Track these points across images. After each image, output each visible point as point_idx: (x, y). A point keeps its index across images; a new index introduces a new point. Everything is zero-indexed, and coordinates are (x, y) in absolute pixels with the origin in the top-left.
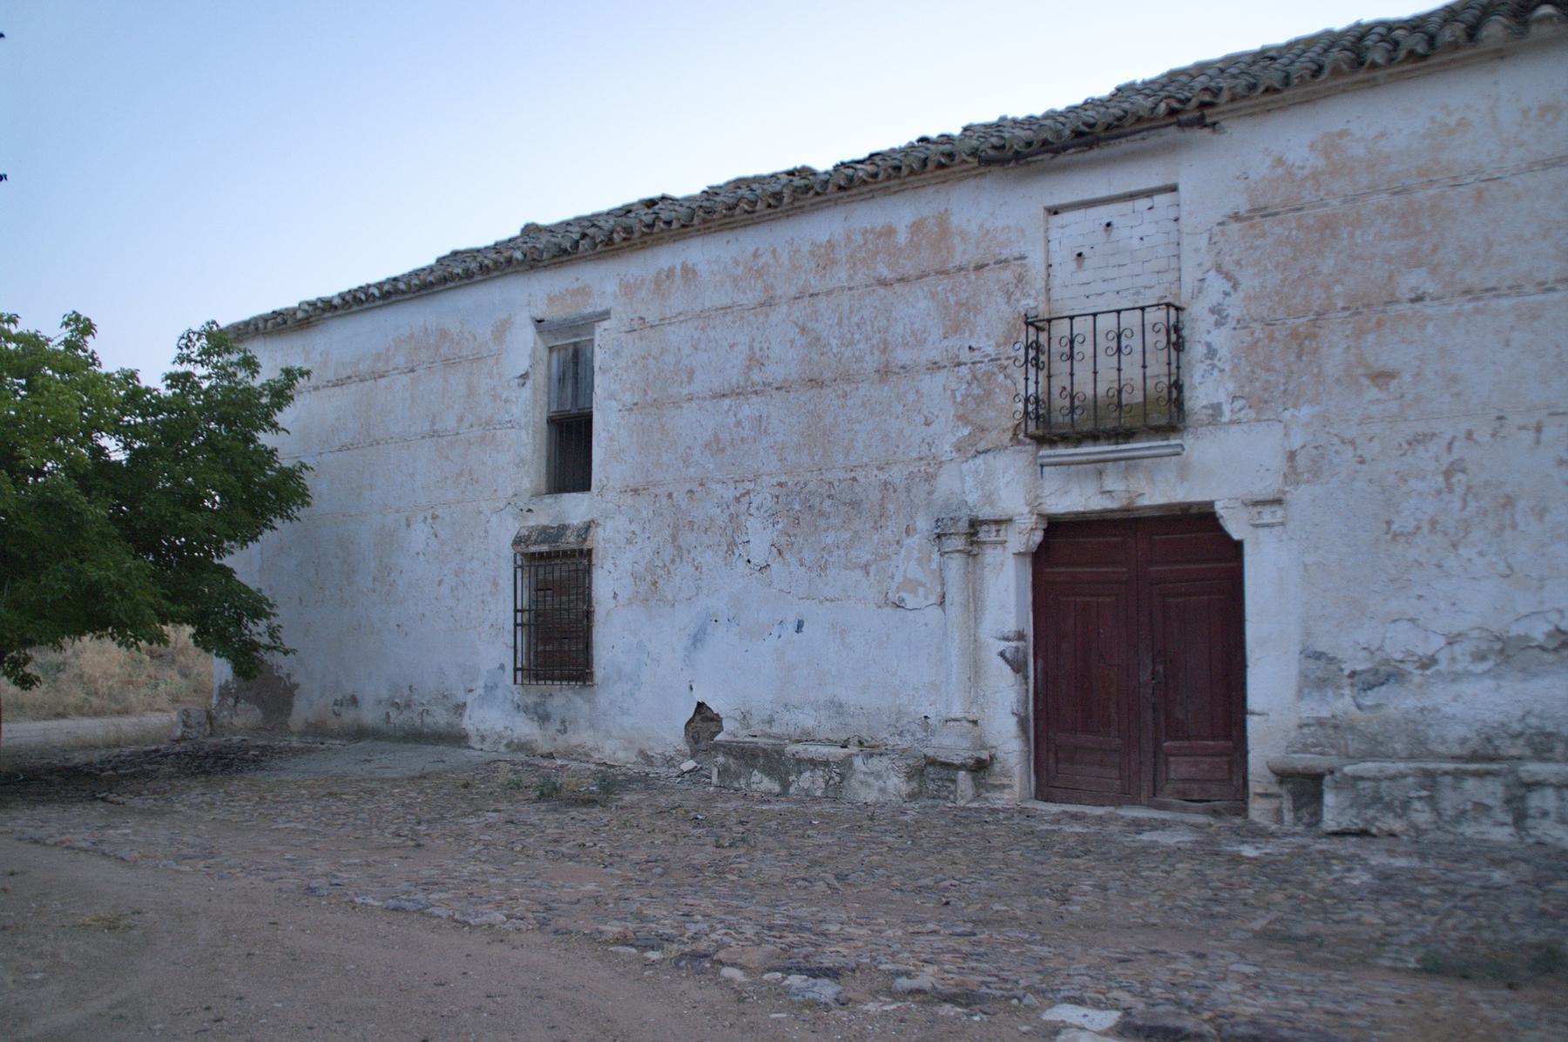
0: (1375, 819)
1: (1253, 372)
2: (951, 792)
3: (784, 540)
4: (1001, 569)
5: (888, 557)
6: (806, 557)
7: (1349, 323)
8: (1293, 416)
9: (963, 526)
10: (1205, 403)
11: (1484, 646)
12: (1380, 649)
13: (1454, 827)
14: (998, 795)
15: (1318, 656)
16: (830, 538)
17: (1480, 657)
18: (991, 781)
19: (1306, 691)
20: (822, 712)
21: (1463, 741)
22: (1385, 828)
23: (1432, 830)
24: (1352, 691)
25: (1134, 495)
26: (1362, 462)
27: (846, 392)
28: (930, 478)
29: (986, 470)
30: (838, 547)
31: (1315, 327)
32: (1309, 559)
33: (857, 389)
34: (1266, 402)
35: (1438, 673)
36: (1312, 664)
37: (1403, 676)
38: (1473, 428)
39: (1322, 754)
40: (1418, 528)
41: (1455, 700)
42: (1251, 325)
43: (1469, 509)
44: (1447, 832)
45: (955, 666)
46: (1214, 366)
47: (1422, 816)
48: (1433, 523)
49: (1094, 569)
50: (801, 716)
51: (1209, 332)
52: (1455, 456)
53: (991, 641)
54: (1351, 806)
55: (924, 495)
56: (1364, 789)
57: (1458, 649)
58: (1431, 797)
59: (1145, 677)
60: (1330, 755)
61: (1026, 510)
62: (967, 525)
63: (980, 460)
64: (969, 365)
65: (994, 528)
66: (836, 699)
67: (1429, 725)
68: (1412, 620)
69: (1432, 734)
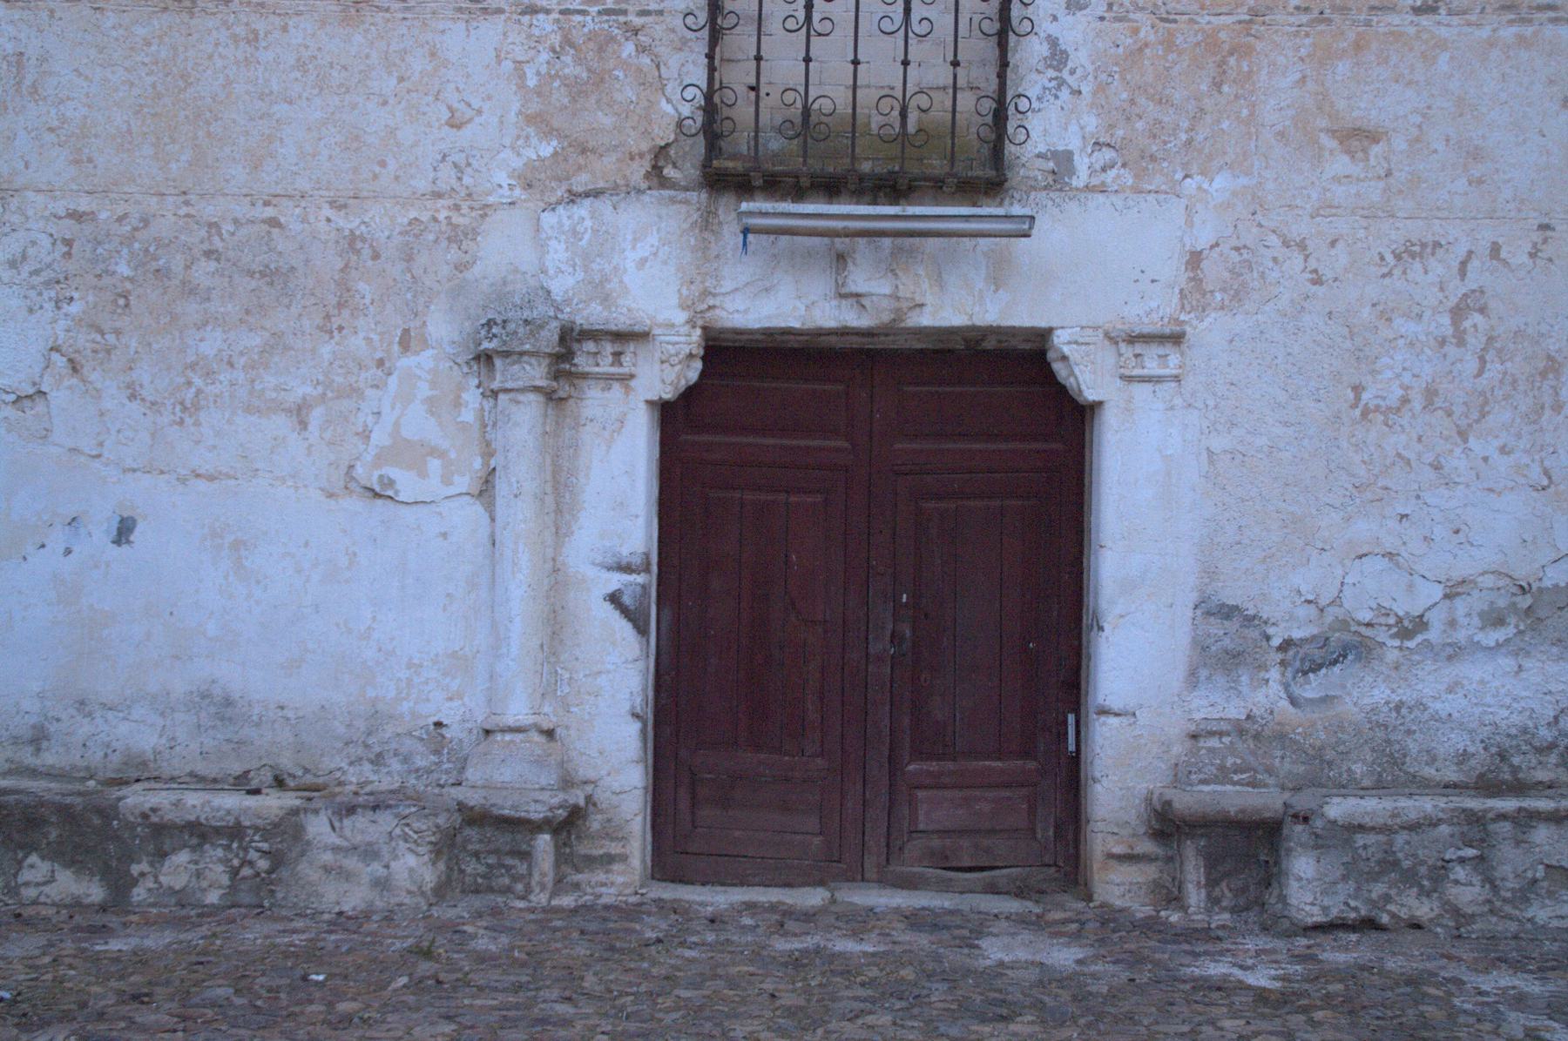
0: (1387, 898)
1: (1132, 102)
2: (516, 878)
3: (84, 339)
4: (619, 431)
5: (354, 392)
6: (146, 379)
7: (1307, 35)
8: (1199, 188)
9: (549, 339)
10: (1042, 148)
11: (1502, 603)
12: (1337, 601)
13: (1516, 907)
14: (601, 876)
15: (1227, 612)
16: (210, 344)
17: (1495, 619)
18: (583, 849)
19: (1203, 673)
20: (180, 716)
21: (1463, 757)
22: (1404, 914)
23: (1481, 915)
24: (1283, 675)
25: (905, 305)
26: (1318, 281)
27: (255, 33)
28: (458, 236)
29: (595, 231)
30: (231, 365)
31: (1249, 35)
32: (1218, 443)
33: (285, 29)
34: (1153, 158)
35: (1427, 644)
36: (1216, 627)
37: (1370, 650)
38: (1500, 241)
39: (1253, 784)
40: (1405, 401)
41: (1450, 690)
42: (1131, 16)
43: (1486, 375)
44: (1510, 917)
45: (518, 619)
46: (1061, 83)
47: (1467, 891)
48: (1430, 394)
49: (786, 442)
50: (124, 728)
51: (1055, 18)
52: (1472, 283)
53: (592, 572)
54: (1345, 878)
55: (445, 270)
56: (1365, 847)
57: (1460, 605)
58: (1481, 858)
59: (880, 645)
60: (1266, 786)
61: (680, 317)
62: (556, 337)
63: (582, 210)
64: (555, 15)
65: (608, 348)
66: (217, 691)
67: (1409, 732)
68: (1390, 555)
69: (1413, 747)
